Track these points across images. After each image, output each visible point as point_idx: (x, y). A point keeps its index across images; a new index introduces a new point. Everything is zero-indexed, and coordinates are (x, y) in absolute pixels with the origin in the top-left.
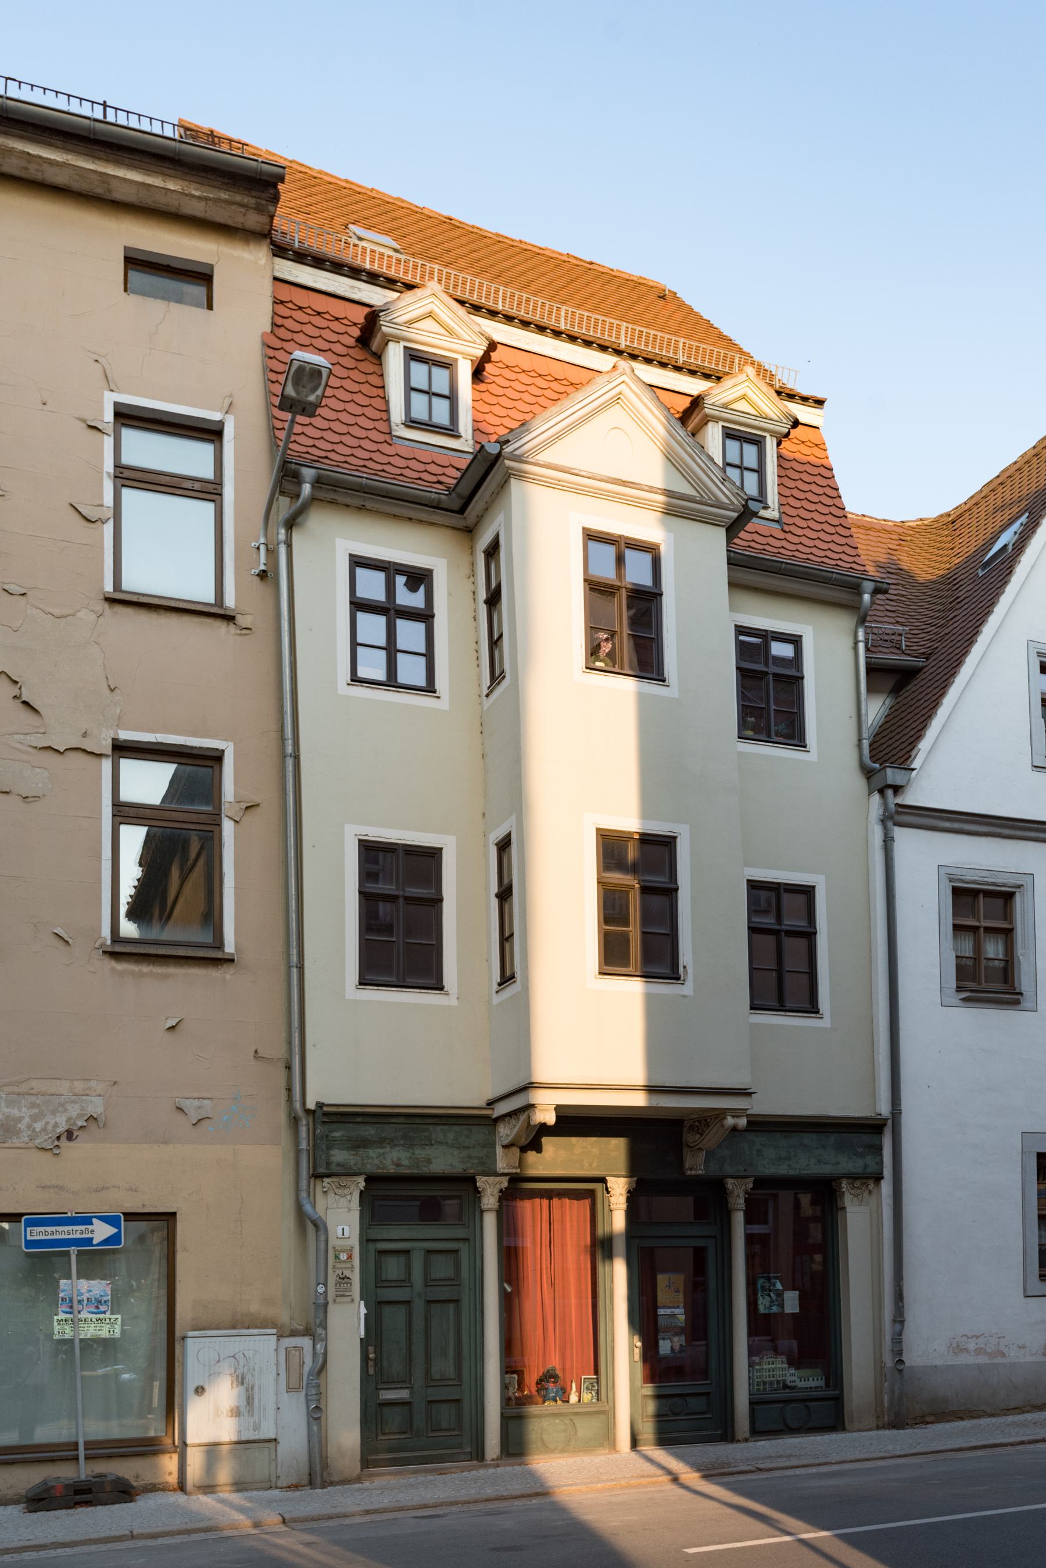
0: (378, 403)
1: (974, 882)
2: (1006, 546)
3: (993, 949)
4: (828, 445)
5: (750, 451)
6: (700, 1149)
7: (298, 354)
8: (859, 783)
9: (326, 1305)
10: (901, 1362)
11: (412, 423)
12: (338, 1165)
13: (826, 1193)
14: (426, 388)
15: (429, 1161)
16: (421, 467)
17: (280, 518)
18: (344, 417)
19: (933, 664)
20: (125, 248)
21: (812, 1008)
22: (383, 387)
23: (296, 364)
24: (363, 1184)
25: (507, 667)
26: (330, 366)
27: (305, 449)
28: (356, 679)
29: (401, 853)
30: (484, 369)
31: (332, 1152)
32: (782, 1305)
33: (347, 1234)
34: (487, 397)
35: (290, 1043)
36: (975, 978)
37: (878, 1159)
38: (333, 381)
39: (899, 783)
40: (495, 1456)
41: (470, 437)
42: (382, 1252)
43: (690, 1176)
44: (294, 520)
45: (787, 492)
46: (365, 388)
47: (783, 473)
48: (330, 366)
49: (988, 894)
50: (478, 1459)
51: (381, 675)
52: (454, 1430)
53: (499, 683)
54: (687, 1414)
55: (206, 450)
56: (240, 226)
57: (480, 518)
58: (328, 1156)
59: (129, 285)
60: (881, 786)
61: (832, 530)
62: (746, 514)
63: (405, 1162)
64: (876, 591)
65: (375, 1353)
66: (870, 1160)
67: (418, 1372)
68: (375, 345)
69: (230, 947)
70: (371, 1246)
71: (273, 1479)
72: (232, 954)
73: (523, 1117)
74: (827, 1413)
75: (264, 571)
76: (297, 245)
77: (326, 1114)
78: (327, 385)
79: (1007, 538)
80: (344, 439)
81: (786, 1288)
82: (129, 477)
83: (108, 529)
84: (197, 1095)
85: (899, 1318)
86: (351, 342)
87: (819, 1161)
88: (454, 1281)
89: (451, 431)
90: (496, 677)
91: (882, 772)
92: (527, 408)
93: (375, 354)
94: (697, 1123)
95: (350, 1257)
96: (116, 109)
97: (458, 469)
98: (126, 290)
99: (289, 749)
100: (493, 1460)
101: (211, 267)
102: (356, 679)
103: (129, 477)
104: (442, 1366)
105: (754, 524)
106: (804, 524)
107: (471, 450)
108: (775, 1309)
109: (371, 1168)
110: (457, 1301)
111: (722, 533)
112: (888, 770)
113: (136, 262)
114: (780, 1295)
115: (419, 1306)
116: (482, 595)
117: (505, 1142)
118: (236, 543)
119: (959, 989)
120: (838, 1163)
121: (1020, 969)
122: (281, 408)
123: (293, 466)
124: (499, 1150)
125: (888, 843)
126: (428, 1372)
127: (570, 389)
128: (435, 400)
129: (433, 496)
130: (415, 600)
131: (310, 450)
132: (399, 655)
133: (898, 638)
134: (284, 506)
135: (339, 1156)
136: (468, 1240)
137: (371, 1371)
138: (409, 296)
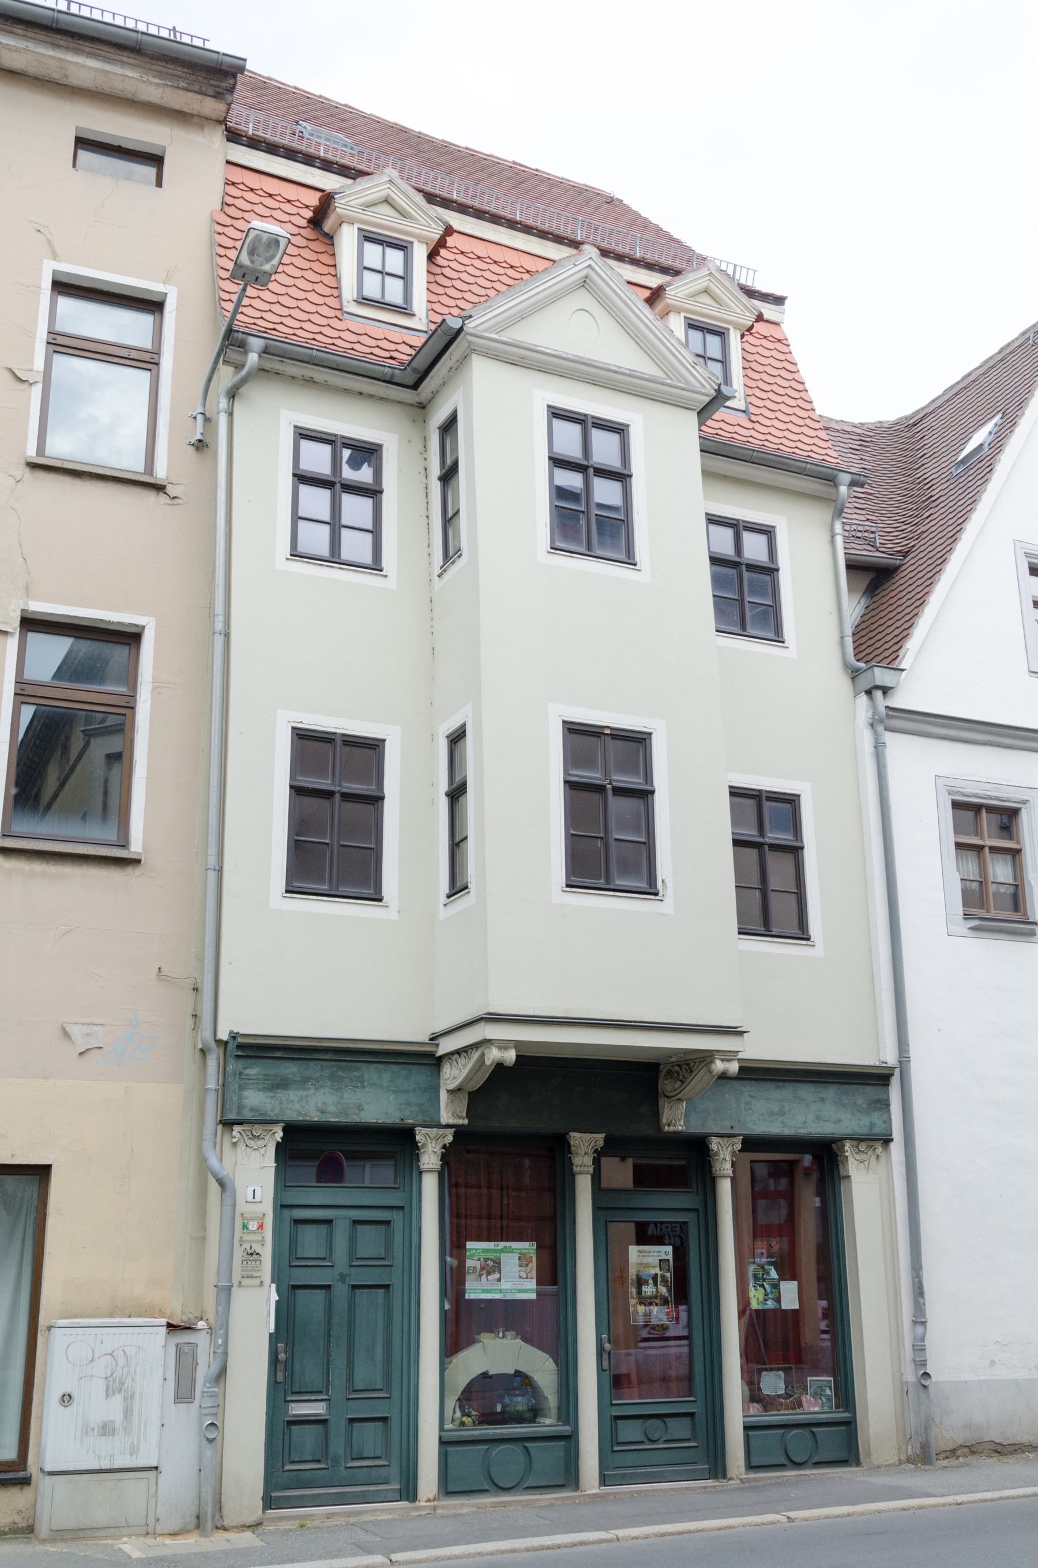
0: (329, 280)
1: (976, 796)
2: (981, 445)
3: (1000, 871)
4: (790, 341)
5: (714, 341)
6: (679, 1099)
7: (256, 223)
8: (842, 683)
9: (229, 1289)
10: (926, 1375)
11: (365, 301)
12: (252, 1110)
13: (824, 1158)
14: (379, 268)
15: (360, 1108)
16: (374, 343)
17: (220, 390)
18: (293, 292)
19: (912, 562)
20: (77, 128)
21: (801, 933)
22: (335, 266)
23: (252, 234)
24: (281, 1134)
25: (464, 545)
26: (289, 236)
27: (252, 321)
28: (296, 554)
29: (339, 743)
30: (438, 254)
31: (246, 1093)
32: (778, 1300)
33: (258, 1198)
34: (441, 280)
35: (201, 960)
36: (983, 904)
37: (886, 1116)
38: (291, 250)
39: (887, 684)
40: (431, 1497)
41: (424, 316)
42: (298, 1222)
43: (668, 1132)
44: (238, 389)
45: (753, 384)
46: (316, 266)
47: (747, 365)
48: (289, 236)
49: (991, 809)
50: (408, 1500)
51: (323, 549)
52: (379, 1458)
53: (453, 563)
54: (667, 1441)
55: (145, 321)
56: (195, 112)
57: (435, 394)
58: (240, 1098)
59: (78, 162)
60: (867, 688)
61: (800, 422)
62: (719, 399)
63: (332, 1109)
64: (853, 484)
65: (286, 1352)
66: (876, 1117)
67: (338, 1378)
68: (328, 226)
69: (136, 847)
70: (288, 1214)
71: (151, 1521)
72: (140, 854)
73: (476, 1055)
74: (838, 1442)
75: (200, 441)
76: (250, 133)
77: (240, 1046)
78: (285, 253)
79: (980, 437)
80: (293, 312)
81: (782, 1277)
82: (62, 344)
83: (37, 392)
84: (87, 1020)
85: (920, 1319)
86: (304, 223)
87: (818, 1118)
88: (382, 1262)
89: (404, 310)
90: (450, 554)
91: (870, 672)
92: (482, 292)
93: (326, 234)
94: (677, 1068)
95: (261, 1227)
96: (80, 4)
97: (411, 346)
98: (74, 166)
99: (219, 626)
100: (429, 1500)
101: (164, 149)
102: (296, 554)
103: (62, 344)
104: (367, 1373)
105: (721, 414)
106: (771, 415)
107: (425, 329)
108: (770, 1304)
109: (292, 1115)
110: (386, 1287)
111: (693, 417)
112: (876, 669)
113: (82, 143)
114: (776, 1286)
115: (341, 1291)
116: (436, 471)
117: (451, 1087)
118: (171, 412)
119: (967, 916)
120: (840, 1121)
121: (1032, 895)
122: (232, 278)
123: (240, 335)
124: (443, 1096)
125: (879, 748)
126: (350, 1379)
127: (526, 276)
128: (388, 279)
129: (386, 370)
130: (364, 475)
131: (257, 321)
132: (344, 531)
133: (872, 536)
134: (226, 376)
135: (255, 1099)
136: (402, 1208)
137: (280, 1377)
138: (363, 183)
